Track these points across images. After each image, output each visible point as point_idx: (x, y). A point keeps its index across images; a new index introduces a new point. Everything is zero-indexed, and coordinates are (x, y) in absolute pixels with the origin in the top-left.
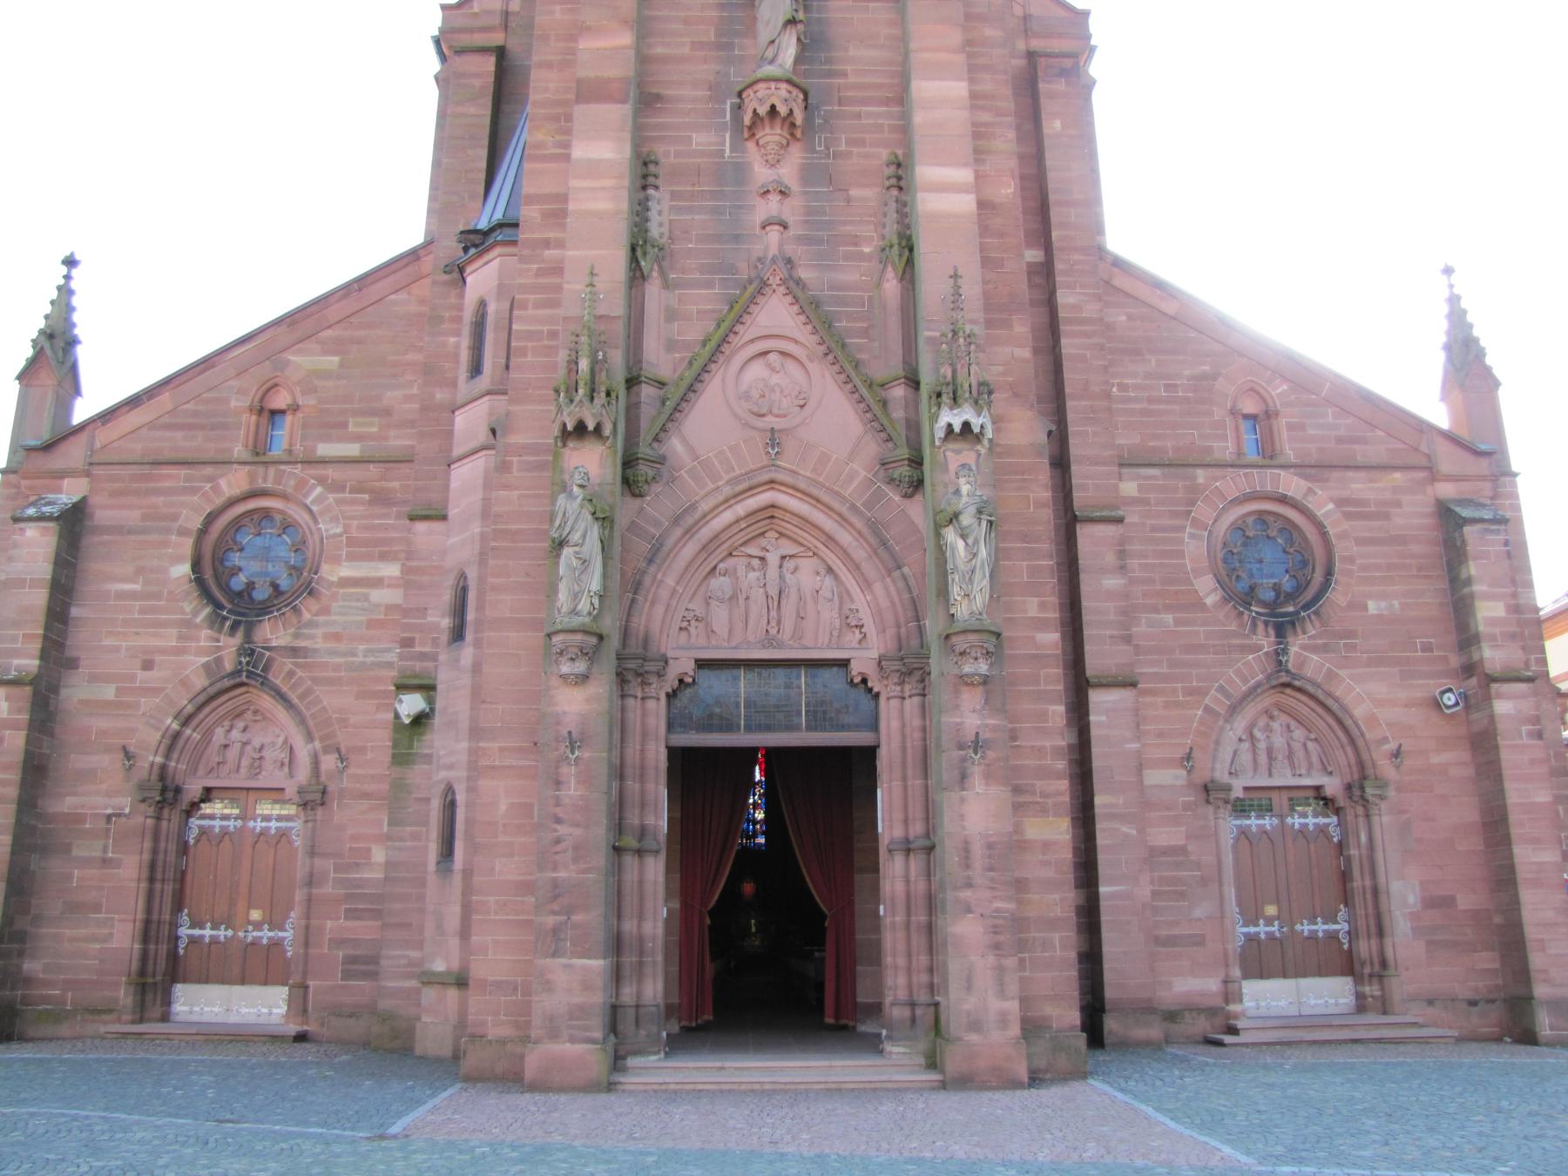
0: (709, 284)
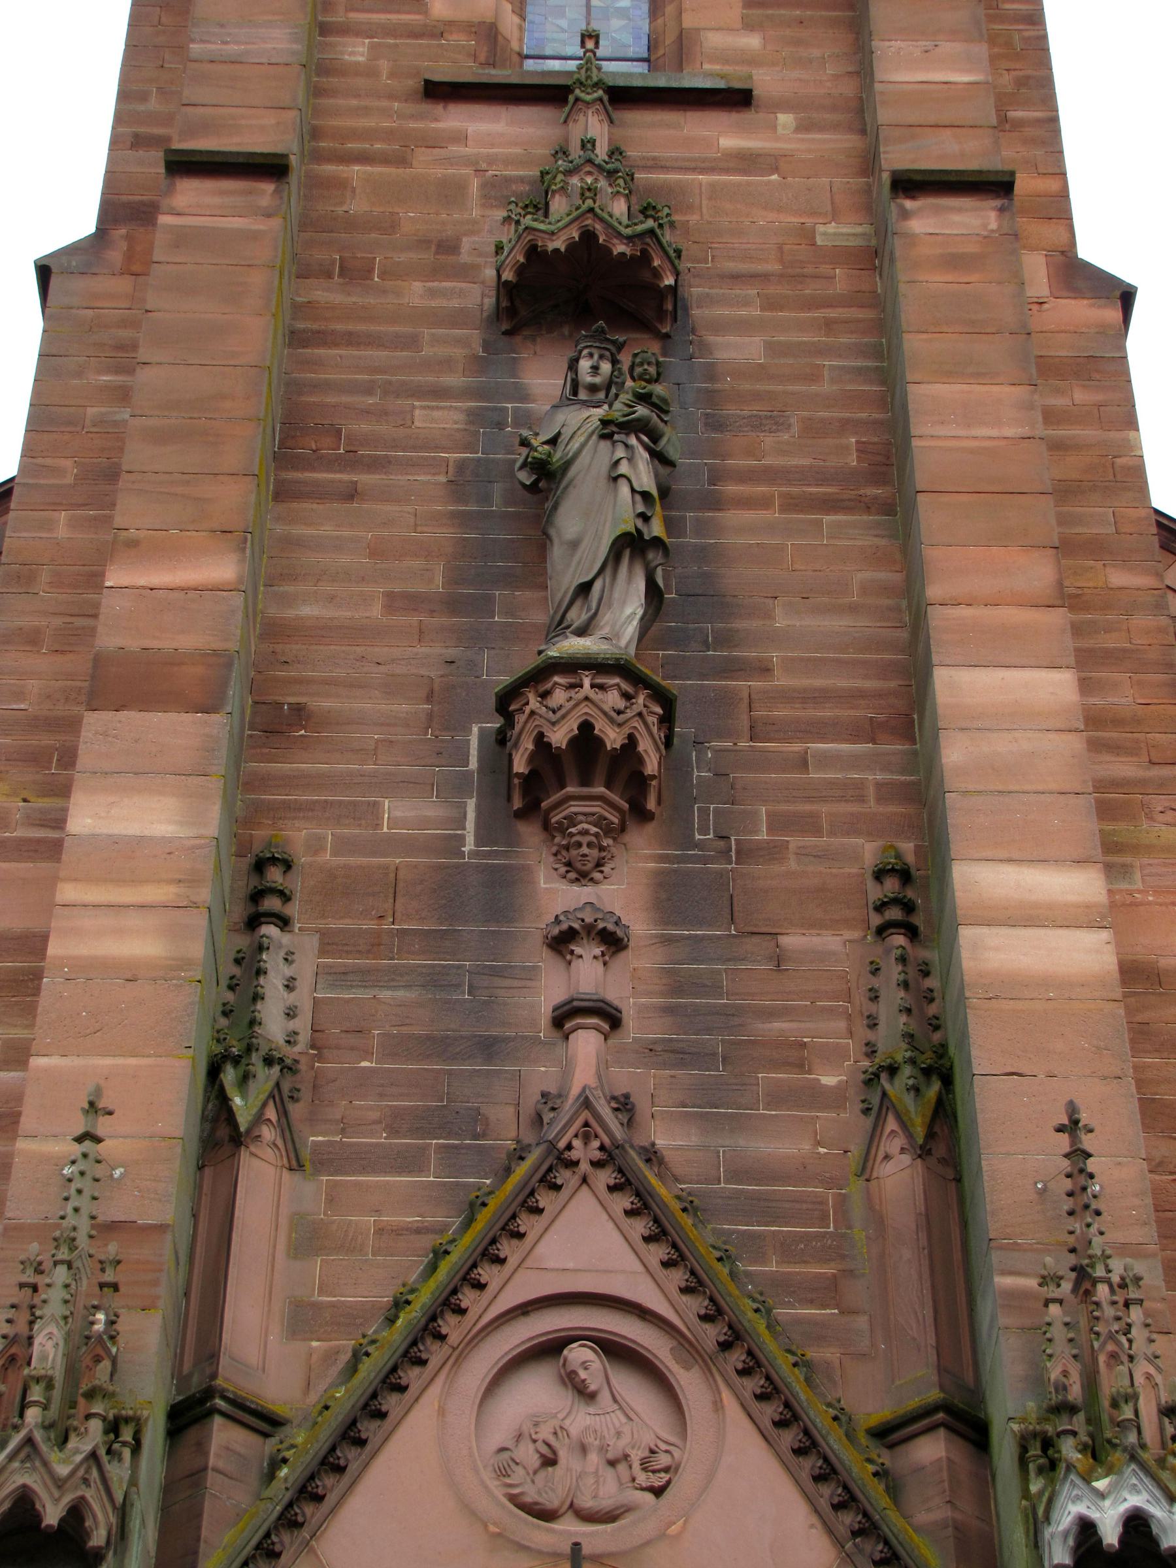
0: (410, 1162)
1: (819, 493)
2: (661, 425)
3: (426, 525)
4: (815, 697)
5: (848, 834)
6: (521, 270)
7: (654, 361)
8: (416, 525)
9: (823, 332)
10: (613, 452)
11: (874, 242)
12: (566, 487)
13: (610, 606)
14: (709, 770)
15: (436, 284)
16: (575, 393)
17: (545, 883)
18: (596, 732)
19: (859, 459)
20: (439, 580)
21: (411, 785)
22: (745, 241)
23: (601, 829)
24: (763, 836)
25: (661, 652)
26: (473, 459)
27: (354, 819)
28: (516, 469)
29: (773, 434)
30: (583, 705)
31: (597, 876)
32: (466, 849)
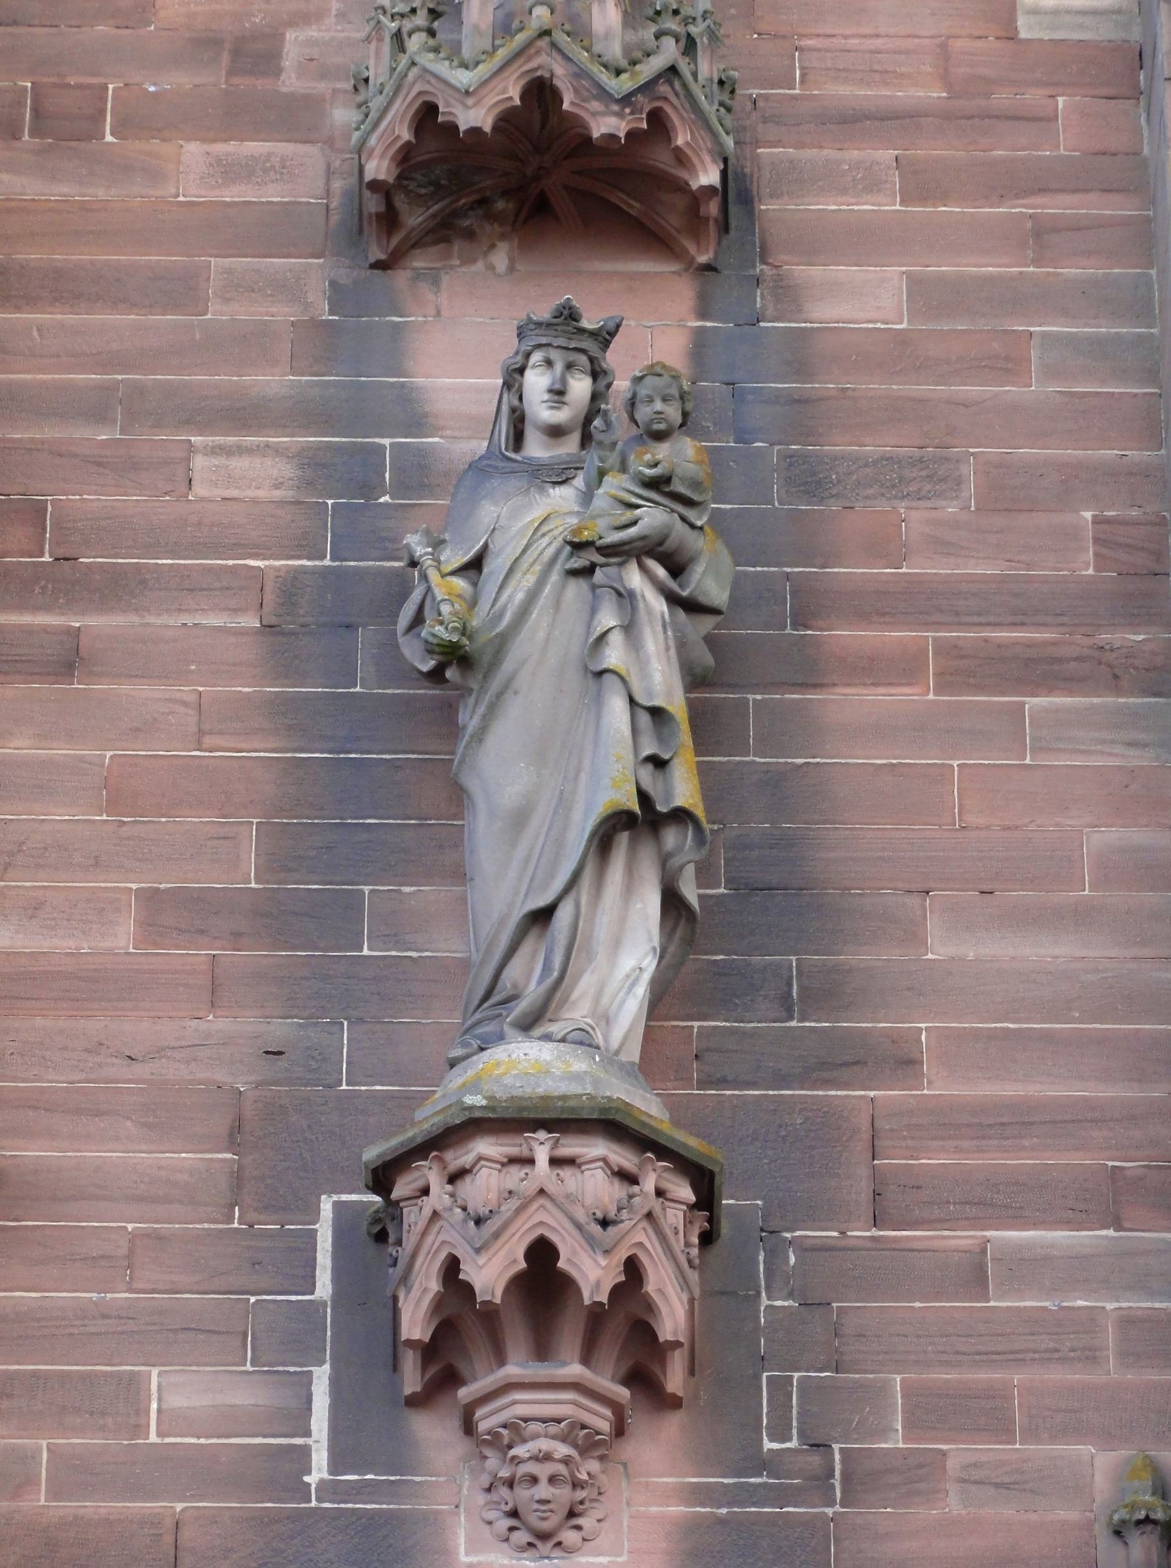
1: (1016, 643)
2: (691, 535)
3: (221, 733)
4: (1003, 1124)
5: (1060, 1434)
6: (405, 157)
7: (675, 392)
8: (201, 733)
9: (1030, 253)
10: (593, 611)
11: (1136, 34)
12: (500, 695)
13: (590, 957)
14: (790, 1295)
15: (231, 147)
16: (518, 439)
17: (467, 1554)
18: (559, 1265)
19: (1101, 561)
20: (251, 862)
21: (202, 1337)
22: (868, 30)
23: (575, 1446)
24: (897, 1442)
25: (696, 1024)
26: (314, 571)
27: (92, 1414)
28: (399, 633)
29: (922, 503)
30: (535, 1205)
31: (570, 1537)
32: (312, 1479)
